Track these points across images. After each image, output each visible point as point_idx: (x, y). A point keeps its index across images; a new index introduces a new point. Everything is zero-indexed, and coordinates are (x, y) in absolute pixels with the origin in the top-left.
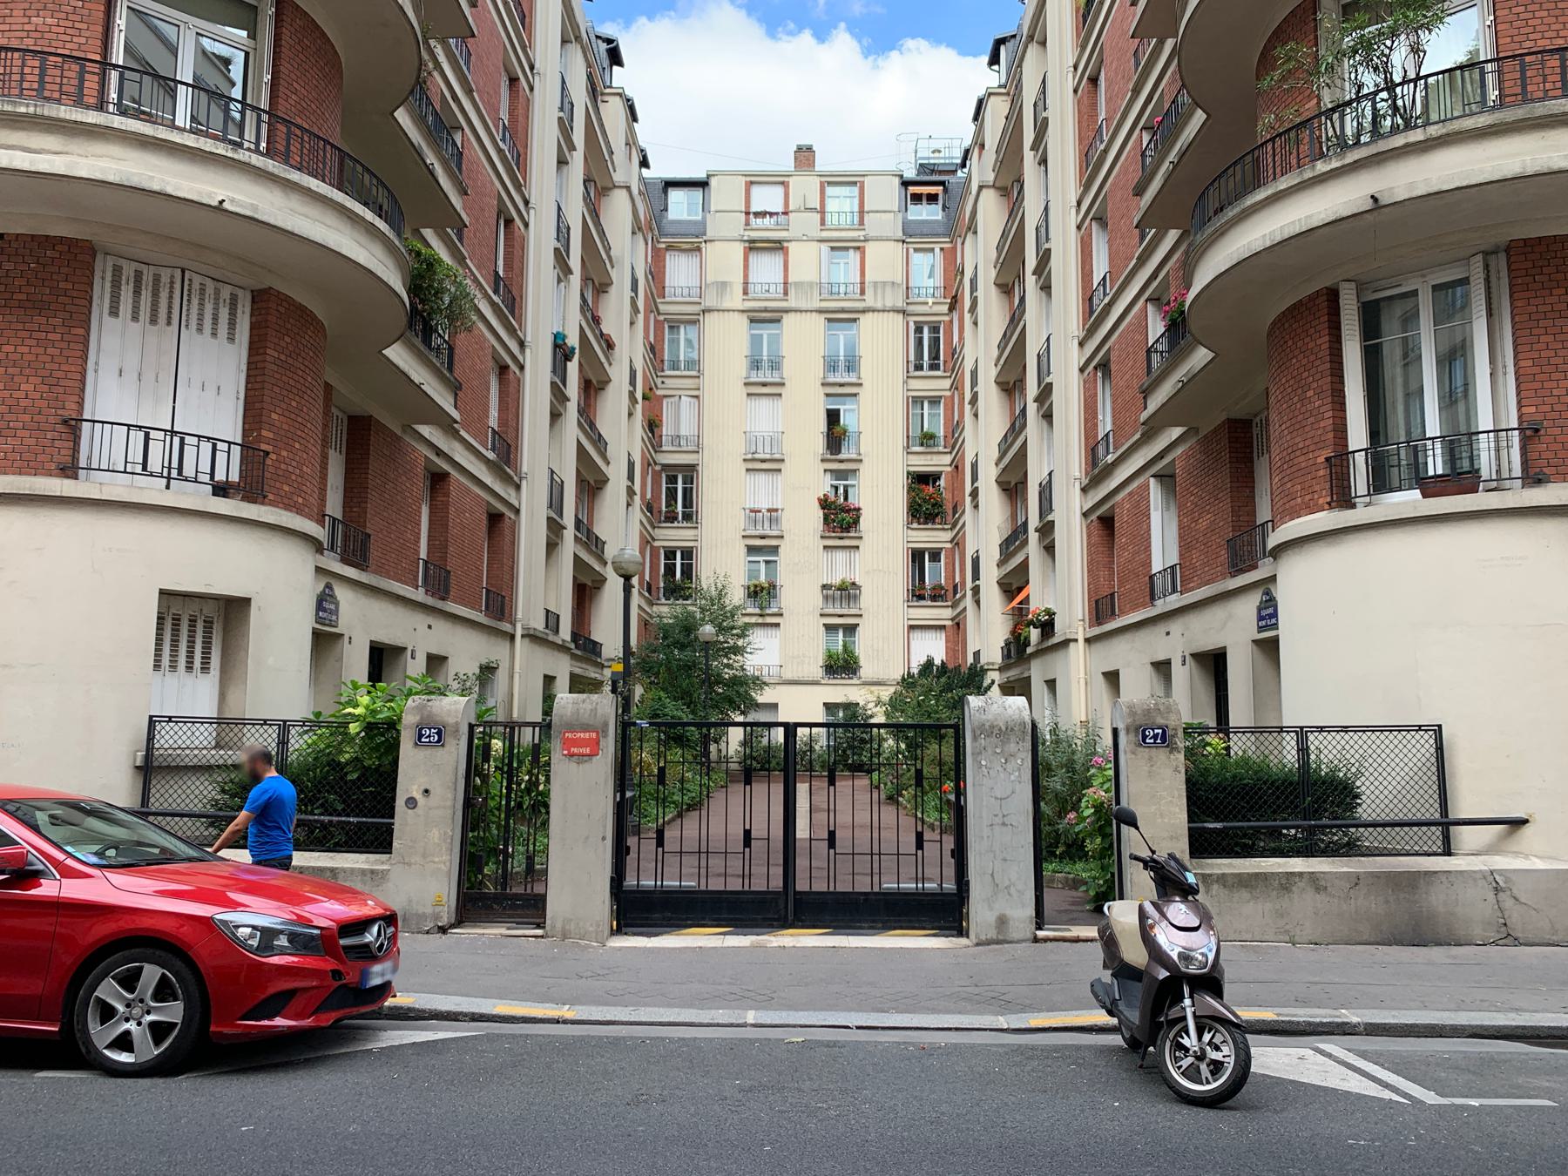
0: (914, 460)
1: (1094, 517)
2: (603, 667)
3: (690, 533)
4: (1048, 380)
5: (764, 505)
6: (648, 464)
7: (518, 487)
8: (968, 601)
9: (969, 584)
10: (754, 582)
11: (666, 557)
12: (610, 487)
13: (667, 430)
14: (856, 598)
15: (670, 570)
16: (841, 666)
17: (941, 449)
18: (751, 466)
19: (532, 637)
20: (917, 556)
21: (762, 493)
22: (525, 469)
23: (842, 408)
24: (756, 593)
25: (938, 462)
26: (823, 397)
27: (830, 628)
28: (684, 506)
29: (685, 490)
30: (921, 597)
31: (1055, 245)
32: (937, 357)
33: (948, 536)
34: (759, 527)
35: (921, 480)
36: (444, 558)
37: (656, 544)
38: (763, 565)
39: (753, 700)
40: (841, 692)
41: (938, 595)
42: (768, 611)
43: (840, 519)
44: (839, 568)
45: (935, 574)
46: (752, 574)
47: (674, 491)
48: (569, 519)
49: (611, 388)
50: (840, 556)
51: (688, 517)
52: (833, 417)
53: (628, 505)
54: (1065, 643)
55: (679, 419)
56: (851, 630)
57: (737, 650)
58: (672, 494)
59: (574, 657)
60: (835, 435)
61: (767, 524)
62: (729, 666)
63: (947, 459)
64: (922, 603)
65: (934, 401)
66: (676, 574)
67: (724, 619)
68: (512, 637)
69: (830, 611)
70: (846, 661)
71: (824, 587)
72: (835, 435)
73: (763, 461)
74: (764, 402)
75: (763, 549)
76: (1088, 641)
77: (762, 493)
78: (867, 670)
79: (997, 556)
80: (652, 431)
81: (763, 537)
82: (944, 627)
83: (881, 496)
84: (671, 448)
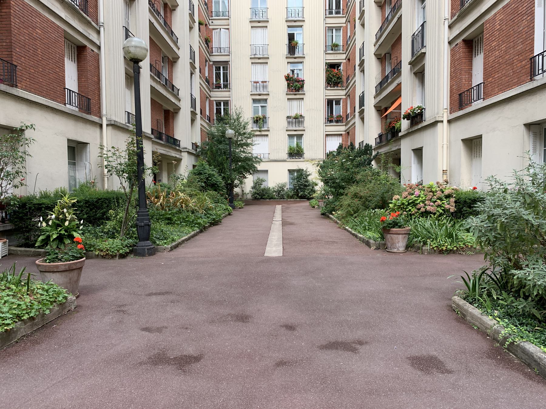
0: (329, 57)
1: (459, 41)
2: (181, 151)
3: (227, 94)
4: (363, 58)
5: (260, 80)
6: (205, 61)
7: (98, 32)
8: (357, 119)
9: (357, 110)
10: (257, 116)
11: (217, 105)
12: (180, 62)
13: (215, 44)
14: (302, 122)
15: (218, 111)
16: (296, 153)
17: (341, 52)
18: (254, 61)
19: (114, 125)
20: (330, 103)
21: (259, 73)
22: (101, 20)
23: (295, 32)
24: (257, 121)
25: (340, 58)
26: (286, 27)
27: (290, 136)
28: (224, 81)
29: (224, 73)
30: (331, 121)
31: (366, 8)
32: (339, 8)
33: (344, 92)
34: (258, 90)
35: (332, 66)
36: (11, 56)
37: (212, 99)
38: (260, 108)
39: (255, 167)
40: (295, 165)
41: (339, 120)
42: (263, 129)
43: (295, 85)
44: (295, 109)
45: (338, 110)
46: (256, 110)
47: (218, 74)
48: (198, 111)
49: (179, 9)
50: (295, 103)
51: (226, 86)
52: (291, 37)
53: (192, 74)
54: (434, 124)
55: (220, 40)
56: (300, 137)
57: (247, 145)
58: (218, 76)
59: (153, 142)
60: (292, 47)
61: (261, 89)
62: (244, 152)
63: (344, 56)
64: (332, 124)
65: (338, 29)
66: (221, 113)
67: (239, 129)
68: (101, 126)
69: (291, 128)
70: (298, 151)
71: (288, 117)
72: (292, 47)
73: (259, 58)
74: (259, 30)
75: (260, 100)
76: (449, 122)
77: (259, 73)
78: (307, 154)
79: (374, 93)
80: (207, 44)
81: (260, 95)
82: (342, 134)
83: (314, 75)
84: (217, 54)
